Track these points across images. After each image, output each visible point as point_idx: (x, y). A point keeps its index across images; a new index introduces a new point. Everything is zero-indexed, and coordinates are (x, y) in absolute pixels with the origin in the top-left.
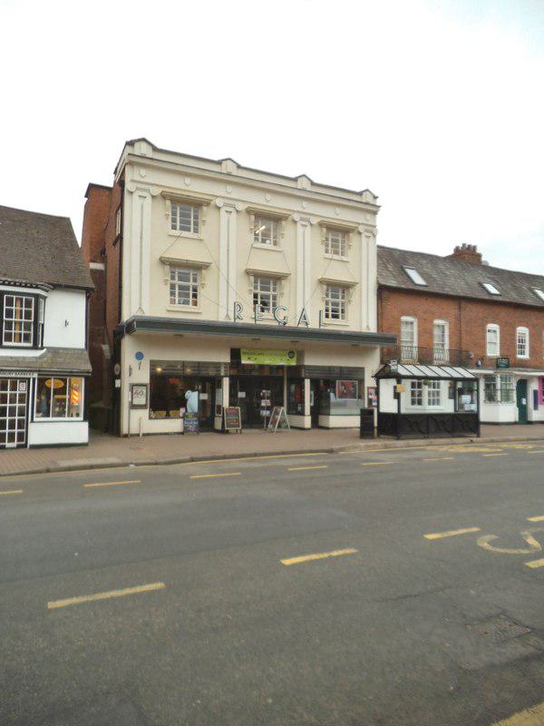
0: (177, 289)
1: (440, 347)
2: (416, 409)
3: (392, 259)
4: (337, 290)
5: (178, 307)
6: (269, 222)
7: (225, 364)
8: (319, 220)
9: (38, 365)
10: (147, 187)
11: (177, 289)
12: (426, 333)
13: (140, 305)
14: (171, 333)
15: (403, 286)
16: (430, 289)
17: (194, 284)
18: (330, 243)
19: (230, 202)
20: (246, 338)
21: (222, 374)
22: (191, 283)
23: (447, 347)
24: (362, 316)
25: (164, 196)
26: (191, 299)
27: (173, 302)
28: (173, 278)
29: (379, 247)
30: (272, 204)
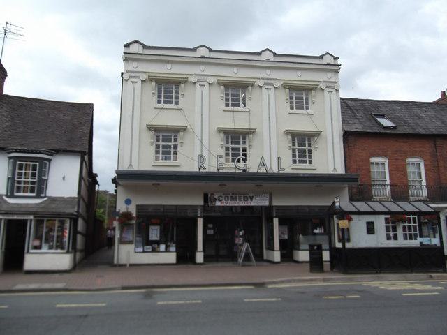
0: (230, 150)
1: (417, 184)
2: (392, 244)
3: (350, 107)
4: (302, 141)
5: (298, 165)
6: (235, 92)
7: (201, 206)
8: (216, 79)
9: (34, 210)
10: (271, 82)
11: (230, 150)
12: (399, 171)
13: (131, 162)
14: (150, 183)
15: (370, 131)
16: (400, 131)
17: (309, 148)
18: (163, 94)
19: (331, 84)
20: (215, 184)
21: (199, 215)
22: (241, 146)
23: (424, 183)
24: (329, 158)
25: (284, 86)
26: (172, 155)
27: (157, 158)
28: (158, 140)
29: (344, 101)
30: (305, 77)
